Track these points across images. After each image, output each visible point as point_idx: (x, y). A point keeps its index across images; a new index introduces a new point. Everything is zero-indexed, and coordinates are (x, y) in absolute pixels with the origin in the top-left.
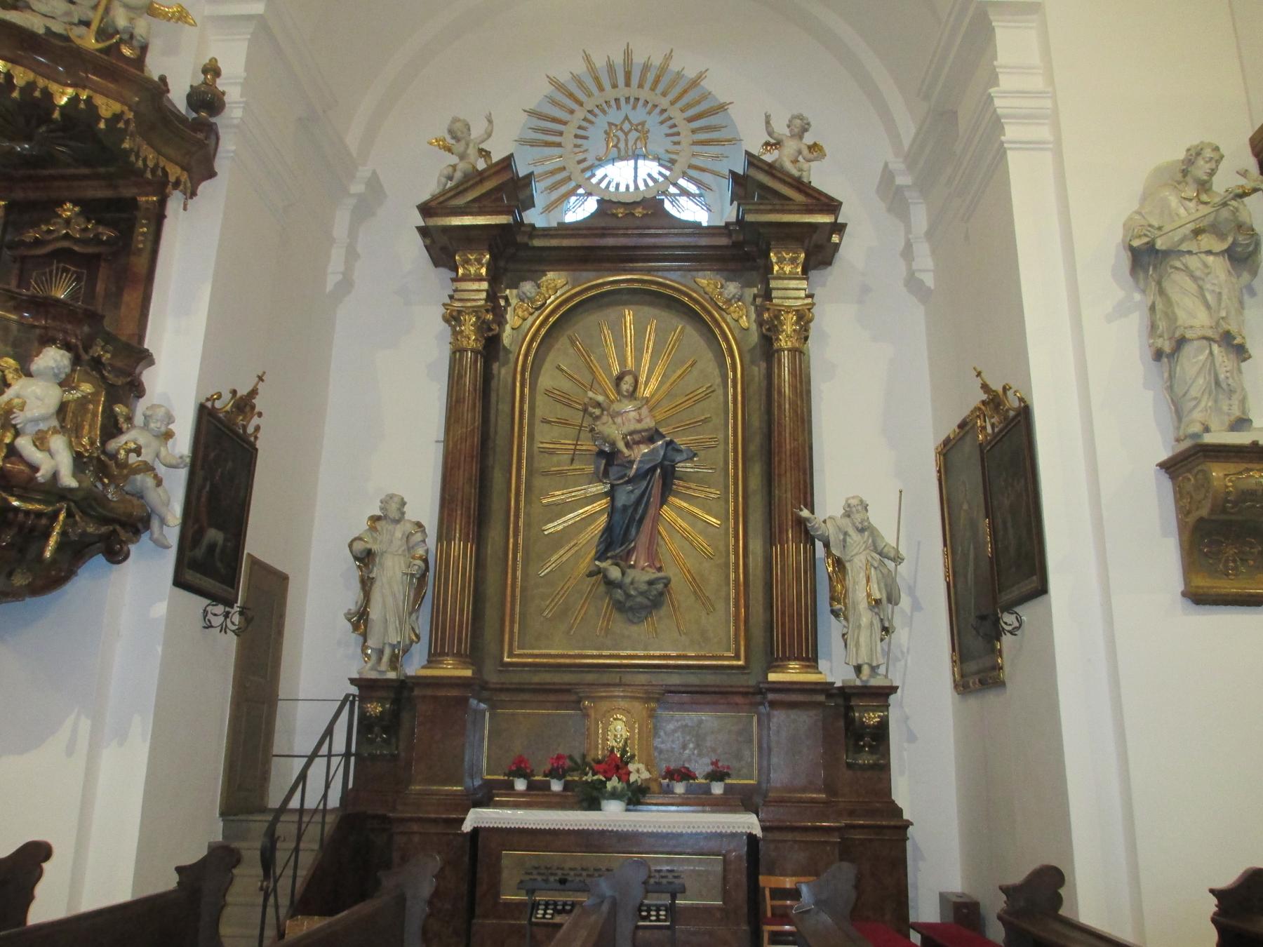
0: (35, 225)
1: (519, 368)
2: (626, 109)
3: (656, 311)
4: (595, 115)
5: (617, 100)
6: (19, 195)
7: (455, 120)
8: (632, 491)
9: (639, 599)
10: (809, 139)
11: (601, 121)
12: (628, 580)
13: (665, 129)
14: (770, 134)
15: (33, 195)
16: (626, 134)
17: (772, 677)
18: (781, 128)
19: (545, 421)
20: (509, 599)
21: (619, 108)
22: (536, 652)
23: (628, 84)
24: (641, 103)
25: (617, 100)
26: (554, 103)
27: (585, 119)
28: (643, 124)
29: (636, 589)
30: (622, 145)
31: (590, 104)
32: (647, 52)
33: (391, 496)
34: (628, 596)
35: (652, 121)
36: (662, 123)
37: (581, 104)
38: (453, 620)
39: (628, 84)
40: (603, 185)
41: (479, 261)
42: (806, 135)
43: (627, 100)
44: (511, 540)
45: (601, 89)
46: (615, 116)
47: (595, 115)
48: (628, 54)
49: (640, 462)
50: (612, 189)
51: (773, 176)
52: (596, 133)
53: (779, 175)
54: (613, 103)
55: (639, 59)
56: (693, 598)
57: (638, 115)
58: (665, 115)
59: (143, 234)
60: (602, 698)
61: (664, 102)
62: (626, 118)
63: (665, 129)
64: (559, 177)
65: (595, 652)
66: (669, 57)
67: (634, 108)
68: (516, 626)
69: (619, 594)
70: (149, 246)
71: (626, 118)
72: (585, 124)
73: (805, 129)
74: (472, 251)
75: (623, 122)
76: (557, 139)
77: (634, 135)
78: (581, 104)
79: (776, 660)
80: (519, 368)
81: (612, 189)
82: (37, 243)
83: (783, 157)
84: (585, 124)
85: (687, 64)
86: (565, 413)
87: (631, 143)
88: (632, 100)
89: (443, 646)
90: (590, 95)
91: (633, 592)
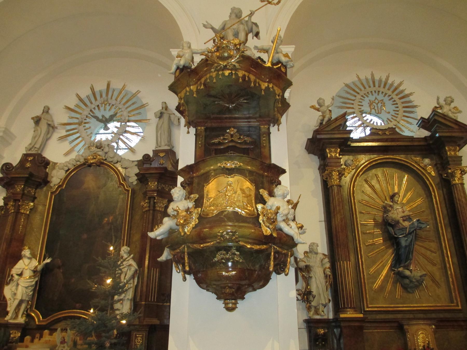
0: (218, 136)
1: (352, 192)
2: (375, 95)
3: (397, 170)
4: (364, 97)
5: (379, 92)
6: (209, 125)
7: (320, 99)
8: (407, 240)
9: (416, 283)
10: (453, 105)
11: (367, 99)
12: (412, 275)
13: (391, 102)
14: (438, 104)
15: (215, 125)
16: (377, 104)
17: (342, 316)
18: (442, 102)
19: (361, 213)
20: (363, 284)
21: (372, 95)
22: (377, 306)
23: (374, 86)
24: (380, 93)
25: (371, 92)
26: (348, 93)
27: (361, 99)
28: (382, 100)
29: (415, 279)
30: (376, 108)
31: (362, 93)
32: (379, 75)
33: (314, 243)
34: (411, 281)
35: (386, 99)
36: (390, 100)
37: (358, 93)
38: (350, 293)
39: (374, 86)
40: (372, 123)
41: (336, 152)
42: (452, 104)
43: (375, 91)
44: (360, 260)
45: (365, 88)
46: (372, 98)
47: (364, 97)
48: (372, 75)
49: (410, 228)
50: (375, 124)
51: (445, 119)
52: (365, 103)
53: (448, 118)
54: (370, 93)
55: (377, 78)
56: (431, 282)
57: (380, 97)
58: (391, 97)
59: (264, 140)
60: (412, 324)
61: (389, 93)
62: (376, 98)
63: (391, 102)
64: (406, 119)
65: (401, 305)
66: (388, 78)
67: (378, 95)
68: (368, 295)
69: (407, 281)
70: (268, 144)
71: (376, 98)
72: (361, 101)
73: (452, 102)
74: (333, 148)
75: (375, 100)
76: (351, 106)
77: (380, 105)
78: (358, 93)
79: (341, 309)
80: (352, 192)
81: (375, 124)
82: (220, 144)
83: (446, 110)
84: (361, 101)
85: (395, 79)
86: (369, 209)
87: (379, 107)
88: (377, 92)
89: (348, 305)
90: (361, 90)
91: (414, 280)
